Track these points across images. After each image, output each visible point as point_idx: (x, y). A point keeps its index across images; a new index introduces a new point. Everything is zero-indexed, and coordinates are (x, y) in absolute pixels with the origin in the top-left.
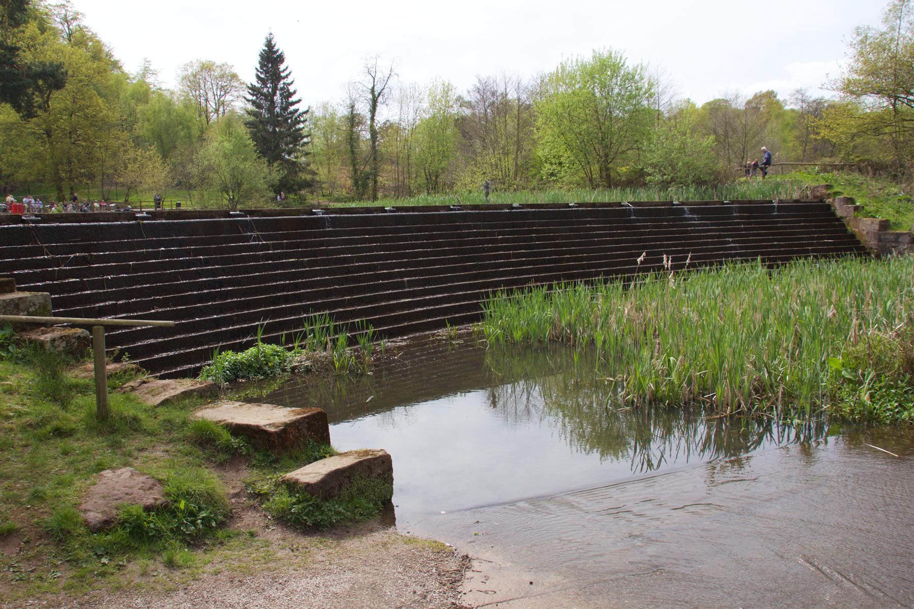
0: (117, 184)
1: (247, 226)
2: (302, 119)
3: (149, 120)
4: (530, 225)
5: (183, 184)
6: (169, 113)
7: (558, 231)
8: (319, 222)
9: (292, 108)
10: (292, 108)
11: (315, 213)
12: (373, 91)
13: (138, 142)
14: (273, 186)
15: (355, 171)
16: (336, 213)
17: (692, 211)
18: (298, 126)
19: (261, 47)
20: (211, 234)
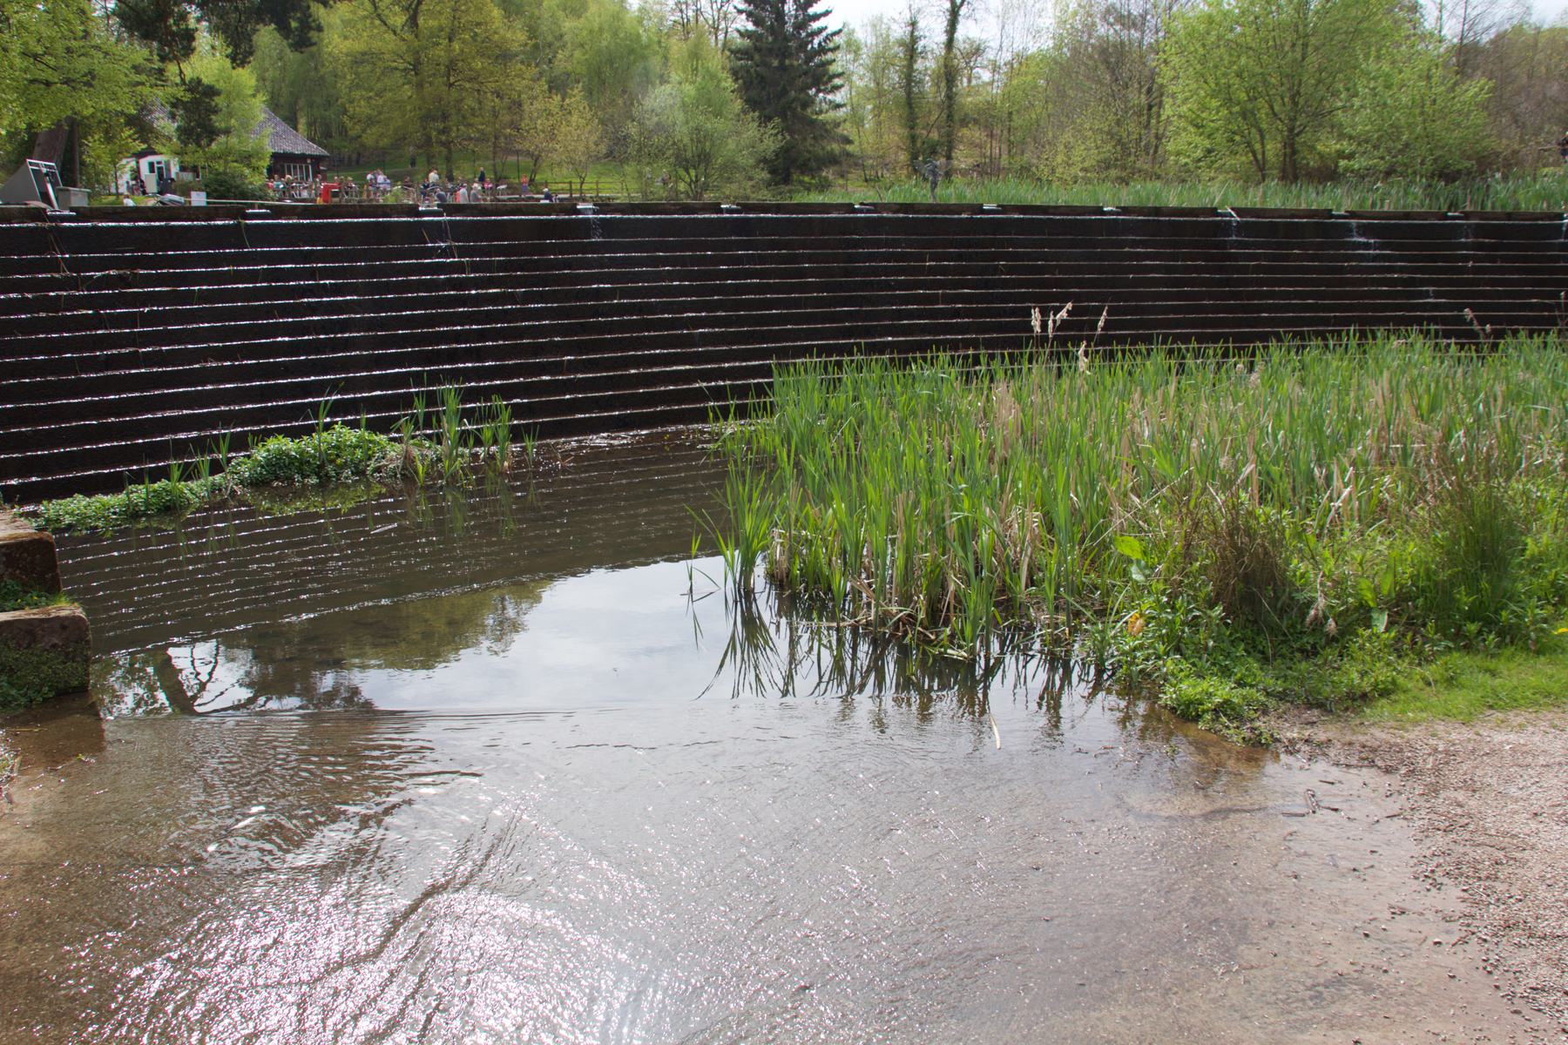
0: (518, 152)
1: (437, 231)
2: (831, 45)
3: (582, 46)
4: (1002, 244)
5: (616, 152)
6: (615, 34)
7: (1057, 257)
8: (585, 227)
9: (815, 25)
10: (815, 25)
11: (579, 212)
13: (558, 86)
14: (765, 160)
15: (913, 138)
16: (623, 213)
17: (1365, 230)
18: (824, 58)
20: (668, 235)
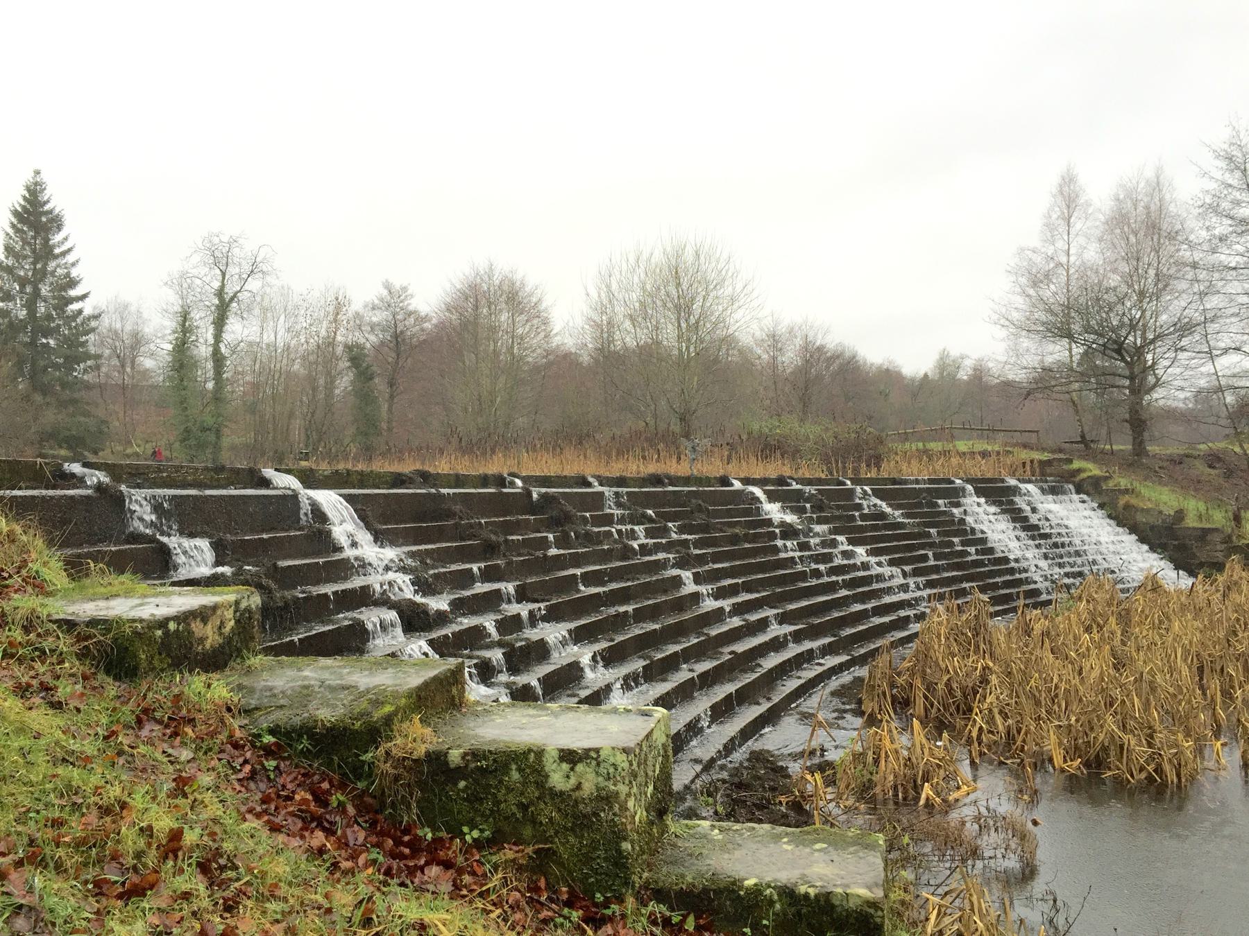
9: (75, 307)
12: (220, 293)
19: (16, 197)
